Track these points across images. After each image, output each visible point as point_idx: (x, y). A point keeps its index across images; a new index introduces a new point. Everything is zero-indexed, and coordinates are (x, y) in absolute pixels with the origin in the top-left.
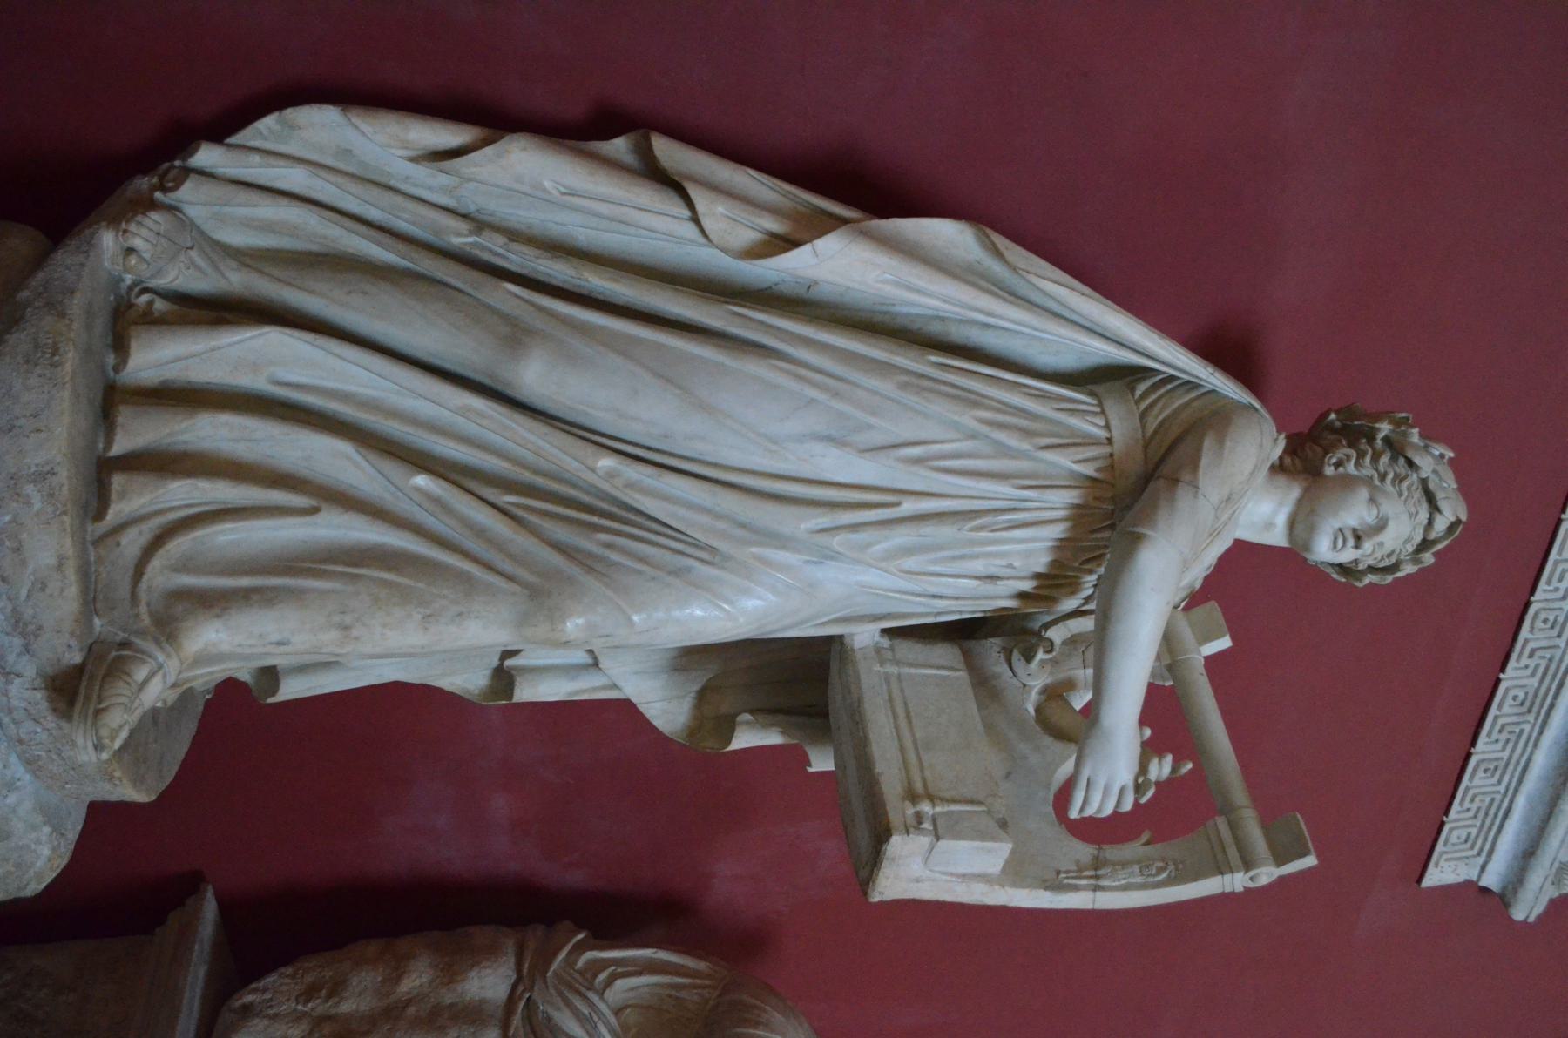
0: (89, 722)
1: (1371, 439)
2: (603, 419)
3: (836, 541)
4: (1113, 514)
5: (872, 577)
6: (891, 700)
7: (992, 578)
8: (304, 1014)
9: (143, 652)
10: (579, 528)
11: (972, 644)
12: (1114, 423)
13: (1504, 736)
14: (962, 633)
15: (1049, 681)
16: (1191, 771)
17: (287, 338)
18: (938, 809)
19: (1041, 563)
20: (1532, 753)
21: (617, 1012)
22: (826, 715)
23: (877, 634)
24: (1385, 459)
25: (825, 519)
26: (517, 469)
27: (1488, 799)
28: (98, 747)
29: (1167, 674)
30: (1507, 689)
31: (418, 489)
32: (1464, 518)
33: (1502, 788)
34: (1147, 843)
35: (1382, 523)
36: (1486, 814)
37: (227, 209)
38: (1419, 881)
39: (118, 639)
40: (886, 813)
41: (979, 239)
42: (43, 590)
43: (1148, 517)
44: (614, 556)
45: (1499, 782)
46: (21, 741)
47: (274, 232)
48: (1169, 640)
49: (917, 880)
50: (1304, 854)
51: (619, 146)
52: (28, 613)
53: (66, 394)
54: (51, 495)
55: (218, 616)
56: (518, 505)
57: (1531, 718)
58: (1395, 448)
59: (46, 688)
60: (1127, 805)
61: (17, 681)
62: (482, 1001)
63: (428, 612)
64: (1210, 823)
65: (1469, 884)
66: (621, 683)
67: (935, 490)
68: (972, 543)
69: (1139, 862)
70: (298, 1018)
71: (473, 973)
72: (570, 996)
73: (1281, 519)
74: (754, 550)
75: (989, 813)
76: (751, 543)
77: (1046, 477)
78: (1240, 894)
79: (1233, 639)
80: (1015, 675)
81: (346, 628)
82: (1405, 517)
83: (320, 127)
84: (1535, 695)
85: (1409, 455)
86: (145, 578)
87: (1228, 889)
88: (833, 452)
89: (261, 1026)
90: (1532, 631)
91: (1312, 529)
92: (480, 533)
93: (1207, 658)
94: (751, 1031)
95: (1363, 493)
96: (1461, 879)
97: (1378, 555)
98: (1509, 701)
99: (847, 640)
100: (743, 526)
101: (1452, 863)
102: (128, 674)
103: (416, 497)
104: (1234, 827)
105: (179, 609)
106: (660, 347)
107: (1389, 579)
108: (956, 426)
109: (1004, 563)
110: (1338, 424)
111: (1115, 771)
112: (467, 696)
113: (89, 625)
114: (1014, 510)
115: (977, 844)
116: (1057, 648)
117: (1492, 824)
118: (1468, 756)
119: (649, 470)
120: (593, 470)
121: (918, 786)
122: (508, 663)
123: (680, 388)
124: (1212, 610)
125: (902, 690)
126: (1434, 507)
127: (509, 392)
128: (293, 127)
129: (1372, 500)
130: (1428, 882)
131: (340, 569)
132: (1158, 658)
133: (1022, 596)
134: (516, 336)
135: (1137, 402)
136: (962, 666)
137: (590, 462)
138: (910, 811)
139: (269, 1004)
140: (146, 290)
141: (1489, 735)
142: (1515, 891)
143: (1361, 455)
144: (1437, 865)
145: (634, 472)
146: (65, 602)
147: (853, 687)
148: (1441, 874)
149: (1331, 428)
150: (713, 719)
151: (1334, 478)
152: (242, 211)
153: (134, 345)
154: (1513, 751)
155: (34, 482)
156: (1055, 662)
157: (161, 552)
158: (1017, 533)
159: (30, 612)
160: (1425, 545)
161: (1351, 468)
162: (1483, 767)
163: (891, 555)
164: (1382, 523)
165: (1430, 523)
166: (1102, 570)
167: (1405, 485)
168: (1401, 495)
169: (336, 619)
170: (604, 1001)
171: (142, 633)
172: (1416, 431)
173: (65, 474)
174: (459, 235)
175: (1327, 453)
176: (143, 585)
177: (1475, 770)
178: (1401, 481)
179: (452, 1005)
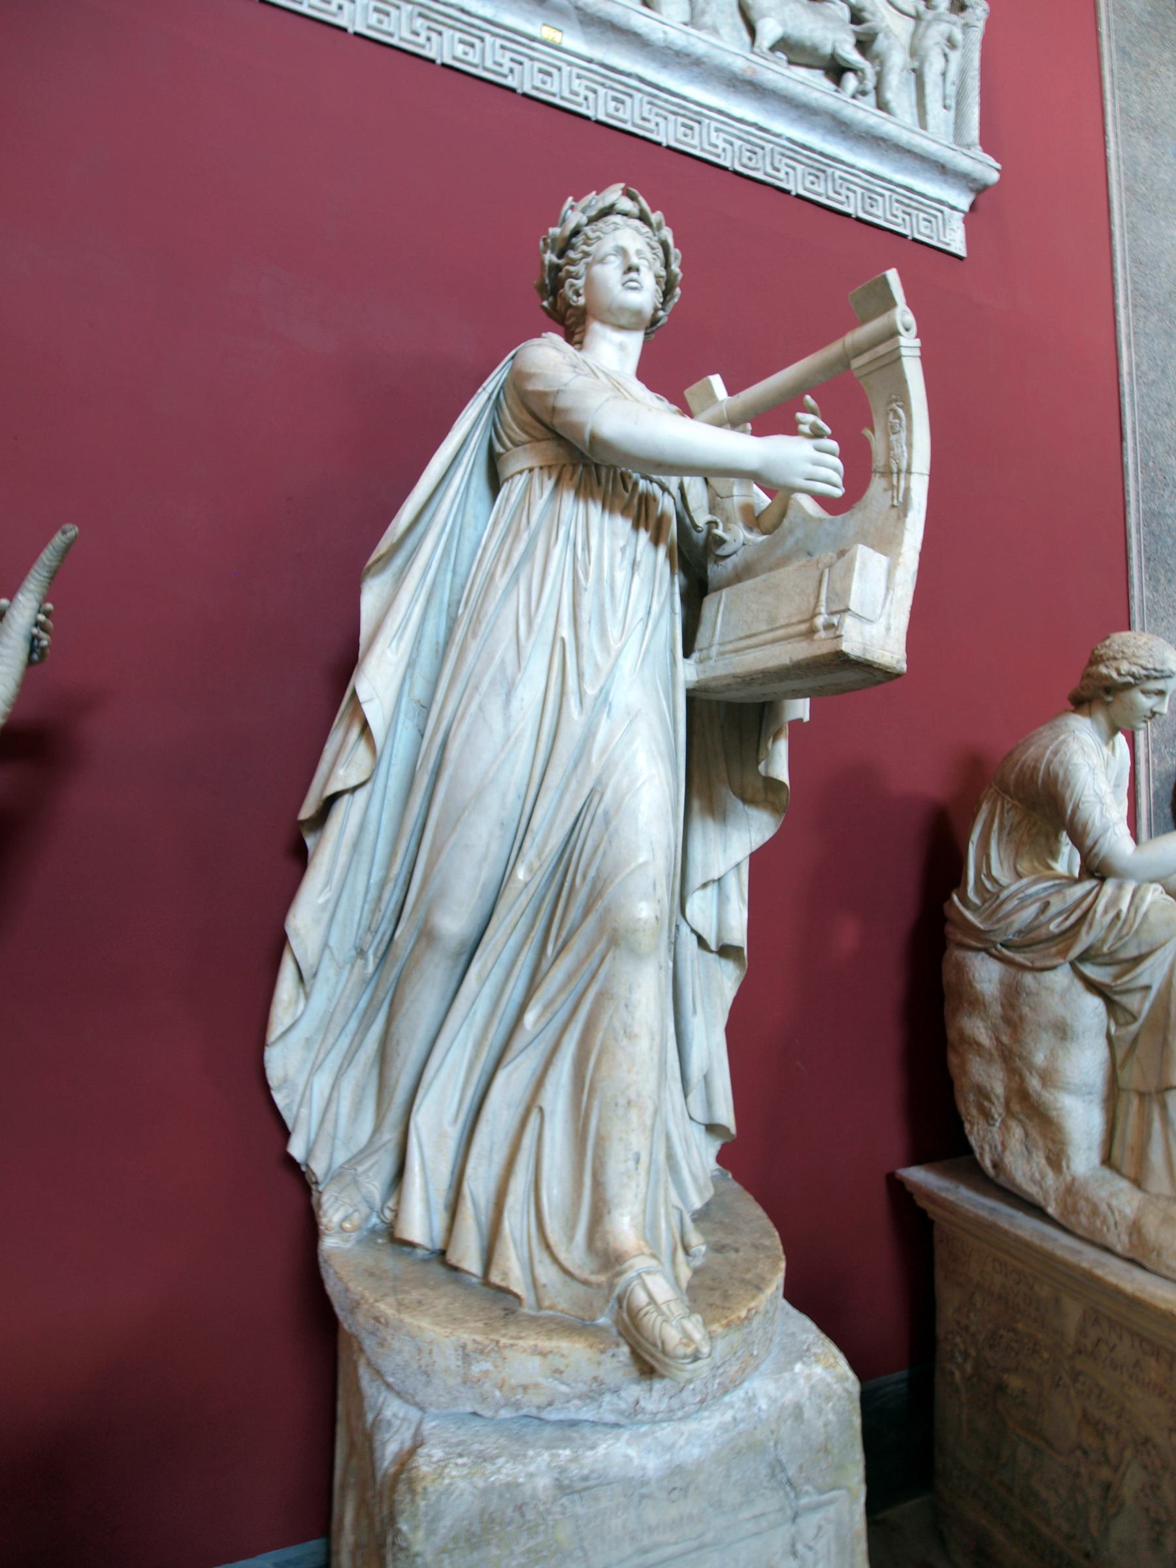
2: (489, 873)
3: (591, 691)
4: (593, 469)
5: (628, 661)
6: (736, 651)
7: (634, 565)
8: (1003, 1121)
10: (571, 902)
11: (710, 587)
12: (518, 468)
13: (844, 191)
15: (741, 524)
17: (423, 1109)
18: (823, 610)
19: (622, 525)
20: (859, 170)
21: (1019, 876)
22: (764, 704)
25: (572, 701)
26: (355, 1015)
27: (896, 205)
30: (805, 189)
32: (622, 185)
33: (887, 193)
34: (873, 431)
35: (626, 256)
37: (341, 1133)
40: (823, 656)
41: (373, 576)
42: (561, 1372)
43: (577, 428)
44: (592, 873)
45: (882, 195)
46: (702, 1401)
49: (888, 629)
50: (885, 282)
51: (310, 841)
52: (581, 1388)
55: (609, 1212)
57: (829, 171)
59: (651, 1379)
60: (834, 445)
61: (642, 1403)
62: (1001, 983)
64: (857, 374)
66: (733, 862)
67: (555, 610)
68: (599, 579)
69: (888, 436)
70: (1005, 1126)
71: (978, 986)
72: (1001, 913)
74: (594, 759)
75: (830, 566)
76: (589, 761)
77: (552, 521)
78: (922, 342)
79: (713, 373)
80: (735, 552)
81: (629, 1103)
82: (618, 233)
83: (284, 1062)
84: (812, 167)
87: (918, 353)
89: (1011, 1159)
91: (623, 309)
92: (570, 977)
94: (1041, 773)
95: (597, 269)
96: (962, 226)
97: (649, 255)
98: (815, 188)
99: (691, 686)
100: (576, 766)
101: (948, 231)
104: (859, 351)
105: (599, 1244)
106: (438, 825)
107: (675, 252)
108: (507, 593)
109: (619, 555)
110: (551, 299)
111: (806, 459)
114: (575, 545)
115: (856, 576)
118: (858, 220)
120: (526, 884)
121: (803, 627)
122: (713, 947)
123: (464, 811)
125: (731, 642)
126: (608, 211)
127: (471, 942)
129: (602, 261)
130: (963, 253)
133: (656, 541)
134: (427, 935)
135: (507, 450)
136: (718, 593)
137: (520, 886)
139: (993, 1148)
140: (382, 1211)
141: (842, 203)
142: (974, 180)
143: (570, 275)
144: (948, 244)
145: (530, 852)
146: (575, 1352)
147: (725, 682)
148: (956, 241)
149: (554, 305)
150: (766, 793)
151: (587, 300)
152: (343, 1121)
155: (470, 1364)
156: (727, 520)
159: (581, 1385)
160: (643, 218)
161: (580, 283)
162: (868, 208)
163: (606, 648)
165: (625, 214)
166: (635, 476)
167: (591, 235)
168: (599, 238)
169: (621, 1111)
170: (1008, 886)
171: (611, 1286)
173: (466, 1336)
174: (365, 966)
175: (570, 306)
176: (576, 1272)
177: (871, 214)
178: (588, 238)
179: (1003, 1006)
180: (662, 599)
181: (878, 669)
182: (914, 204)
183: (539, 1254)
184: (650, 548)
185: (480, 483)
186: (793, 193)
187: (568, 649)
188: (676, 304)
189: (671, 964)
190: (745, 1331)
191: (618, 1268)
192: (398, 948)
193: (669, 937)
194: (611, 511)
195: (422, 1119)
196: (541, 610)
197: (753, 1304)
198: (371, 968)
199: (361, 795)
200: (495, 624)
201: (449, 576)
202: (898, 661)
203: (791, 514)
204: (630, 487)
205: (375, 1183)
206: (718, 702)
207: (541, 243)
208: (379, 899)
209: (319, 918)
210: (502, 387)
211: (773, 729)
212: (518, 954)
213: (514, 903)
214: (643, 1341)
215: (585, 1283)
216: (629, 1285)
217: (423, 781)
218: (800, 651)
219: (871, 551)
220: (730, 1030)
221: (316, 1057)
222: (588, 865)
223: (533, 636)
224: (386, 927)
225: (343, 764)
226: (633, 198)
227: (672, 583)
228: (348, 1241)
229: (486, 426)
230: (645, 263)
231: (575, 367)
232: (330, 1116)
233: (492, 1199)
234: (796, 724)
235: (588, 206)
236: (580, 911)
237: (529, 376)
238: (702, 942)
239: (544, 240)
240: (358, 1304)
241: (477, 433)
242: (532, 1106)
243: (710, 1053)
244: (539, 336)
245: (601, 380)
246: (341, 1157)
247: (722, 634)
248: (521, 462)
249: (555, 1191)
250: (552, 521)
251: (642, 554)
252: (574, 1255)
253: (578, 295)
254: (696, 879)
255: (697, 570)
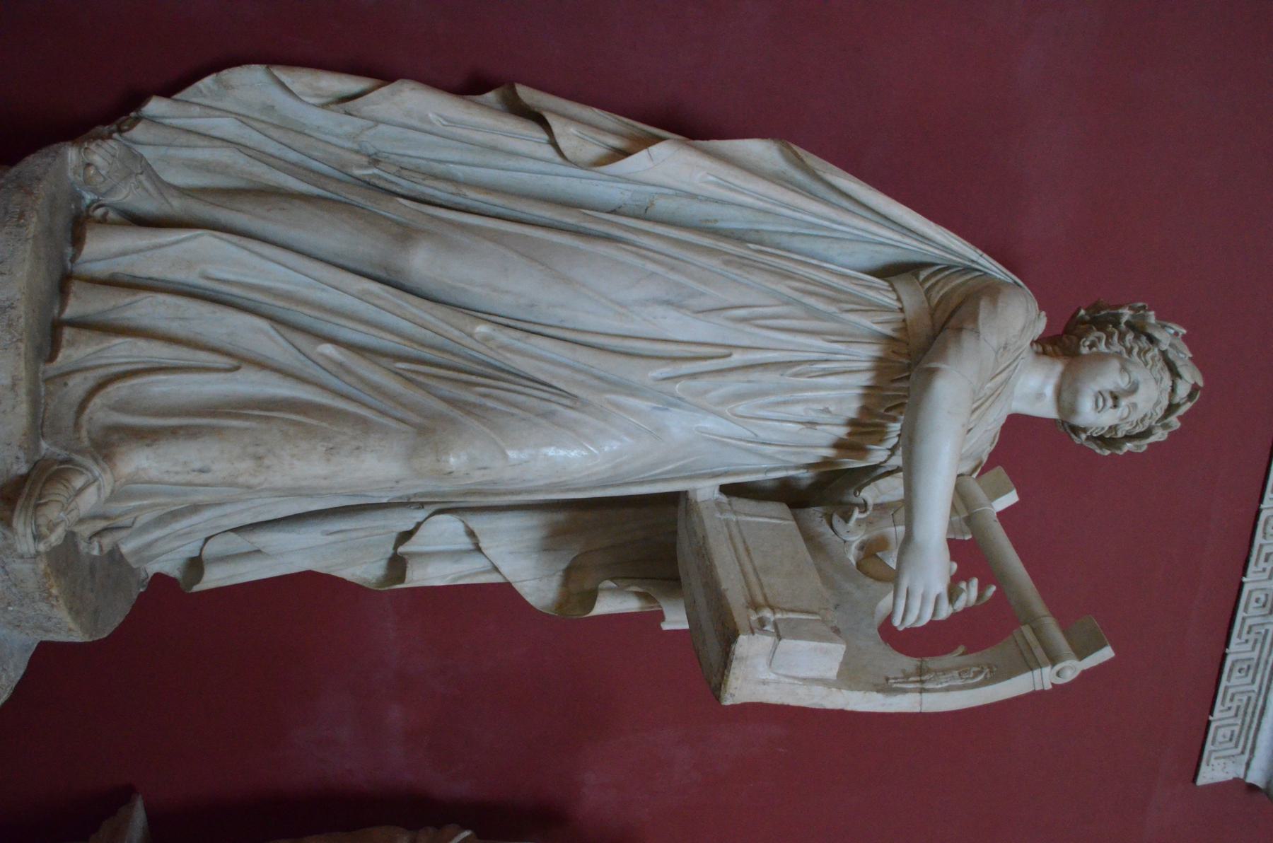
0: (30, 513)
1: (1116, 324)
2: (478, 295)
3: (677, 387)
6: (731, 538)
7: (812, 424)
9: (80, 466)
10: (457, 385)
11: (798, 511)
12: (904, 298)
13: (1252, 636)
14: (788, 494)
15: (865, 538)
16: (995, 592)
17: (216, 242)
18: (779, 616)
19: (851, 409)
22: (678, 579)
23: (717, 491)
24: (1130, 337)
27: (1245, 698)
28: (38, 537)
29: (966, 528)
30: (1250, 592)
31: (322, 355)
32: (1201, 384)
33: (1255, 687)
34: (963, 654)
35: (1132, 394)
36: (1245, 713)
37: (172, 152)
38: (1194, 779)
39: (60, 458)
41: (781, 151)
43: (942, 354)
44: (490, 403)
45: (1253, 681)
47: (208, 171)
48: (961, 494)
49: (764, 683)
50: (1102, 646)
51: (491, 96)
53: (28, 247)
54: (10, 325)
55: (148, 445)
56: (409, 370)
58: (1138, 329)
63: (331, 445)
64: (1016, 632)
65: (1238, 783)
66: (498, 563)
68: (794, 389)
69: (957, 668)
73: (1049, 391)
74: (608, 396)
75: (823, 621)
77: (851, 335)
78: (1048, 692)
80: (836, 533)
82: (1152, 383)
83: (249, 84)
85: (1149, 331)
86: (88, 411)
87: (1038, 688)
88: (673, 314)
90: (1264, 537)
91: (1076, 393)
92: (377, 389)
93: (1000, 514)
95: (1115, 364)
96: (1230, 777)
98: (1253, 604)
99: (691, 495)
101: (1222, 761)
102: (68, 481)
103: (319, 360)
105: (115, 437)
107: (1143, 445)
111: (927, 587)
112: (366, 585)
113: (37, 448)
114: (827, 361)
116: (870, 508)
117: (1251, 721)
119: (518, 334)
120: (471, 336)
121: (760, 599)
122: (401, 549)
124: (999, 473)
125: (740, 532)
128: (227, 87)
129: (1124, 369)
130: (1201, 781)
131: (256, 413)
132: (954, 509)
133: (839, 445)
134: (406, 234)
135: (921, 284)
136: (791, 517)
137: (468, 329)
138: (754, 617)
141: (1239, 636)
143: (1109, 336)
145: (504, 337)
148: (1213, 772)
150: (578, 592)
152: (186, 153)
153: (89, 235)
154: (1261, 652)
157: (102, 393)
158: (831, 380)
160: (1171, 408)
161: (1102, 347)
163: (725, 400)
164: (1132, 394)
165: (1173, 390)
167: (1149, 355)
169: (251, 450)
171: (80, 452)
172: (1152, 313)
174: (361, 167)
175: (1080, 338)
176: (85, 417)
177: (1231, 670)
178: (1145, 353)
180: (780, 456)
181: (723, 675)
182: (1248, 719)
183: (91, 379)
184: (830, 439)
185: (887, 256)
186: (1244, 579)
187: (721, 361)
188: (1093, 451)
189: (385, 501)
190: (37, 595)
191: (100, 458)
192: (384, 201)
193: (415, 495)
194: (864, 396)
195: (205, 242)
196: (757, 331)
197: (61, 601)
198: (358, 172)
199: (549, 152)
200: (741, 284)
201: (789, 229)
202: (732, 695)
203: (878, 586)
204: (892, 413)
205: (133, 196)
206: (675, 532)
207: (1140, 304)
208: (436, 177)
209: (417, 121)
210: (986, 273)
211: (652, 591)
212: (392, 331)
213: (448, 323)
214: (40, 485)
215: (77, 426)
216: (87, 469)
217: (570, 219)
218: (735, 595)
219: (841, 658)
220: (309, 575)
221: (257, 120)
222: (497, 399)
223: (731, 324)
224: (405, 185)
225: (581, 131)
226: (1190, 396)
227: (798, 467)
228: (75, 173)
229: (943, 258)
230: (1125, 414)
231: (1005, 348)
232: (194, 139)
233: (132, 324)
234: (660, 616)
235: (1179, 351)
236: (447, 394)
237: (994, 302)
238: (406, 536)
239: (1144, 307)
240: (30, 193)
241: (937, 252)
242: (240, 360)
243: (282, 554)
244: (1041, 308)
245: (998, 378)
246: (147, 152)
247: (748, 523)
248: (911, 298)
249: (163, 388)
250: (851, 335)
251: (824, 431)
252: (100, 413)
253: (1090, 347)
254: (479, 523)
255: (819, 493)
